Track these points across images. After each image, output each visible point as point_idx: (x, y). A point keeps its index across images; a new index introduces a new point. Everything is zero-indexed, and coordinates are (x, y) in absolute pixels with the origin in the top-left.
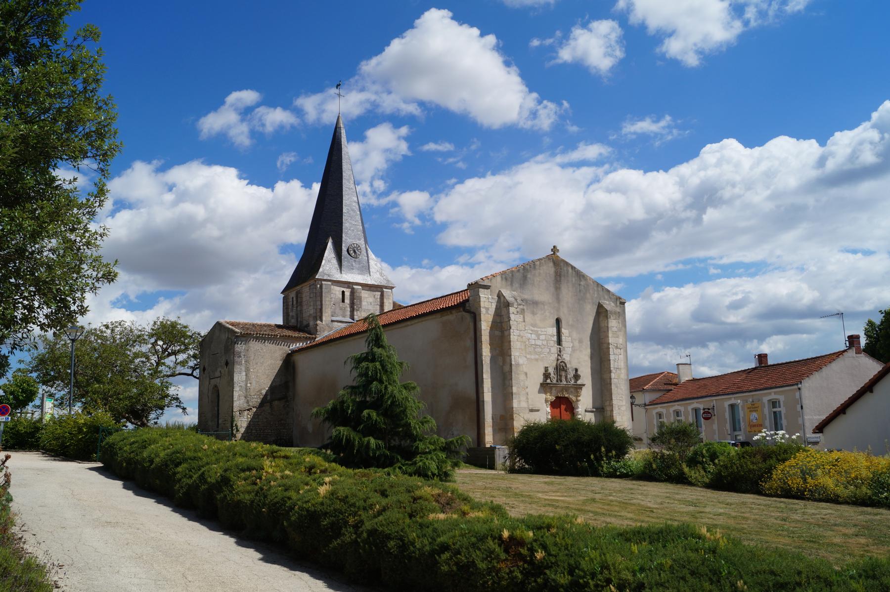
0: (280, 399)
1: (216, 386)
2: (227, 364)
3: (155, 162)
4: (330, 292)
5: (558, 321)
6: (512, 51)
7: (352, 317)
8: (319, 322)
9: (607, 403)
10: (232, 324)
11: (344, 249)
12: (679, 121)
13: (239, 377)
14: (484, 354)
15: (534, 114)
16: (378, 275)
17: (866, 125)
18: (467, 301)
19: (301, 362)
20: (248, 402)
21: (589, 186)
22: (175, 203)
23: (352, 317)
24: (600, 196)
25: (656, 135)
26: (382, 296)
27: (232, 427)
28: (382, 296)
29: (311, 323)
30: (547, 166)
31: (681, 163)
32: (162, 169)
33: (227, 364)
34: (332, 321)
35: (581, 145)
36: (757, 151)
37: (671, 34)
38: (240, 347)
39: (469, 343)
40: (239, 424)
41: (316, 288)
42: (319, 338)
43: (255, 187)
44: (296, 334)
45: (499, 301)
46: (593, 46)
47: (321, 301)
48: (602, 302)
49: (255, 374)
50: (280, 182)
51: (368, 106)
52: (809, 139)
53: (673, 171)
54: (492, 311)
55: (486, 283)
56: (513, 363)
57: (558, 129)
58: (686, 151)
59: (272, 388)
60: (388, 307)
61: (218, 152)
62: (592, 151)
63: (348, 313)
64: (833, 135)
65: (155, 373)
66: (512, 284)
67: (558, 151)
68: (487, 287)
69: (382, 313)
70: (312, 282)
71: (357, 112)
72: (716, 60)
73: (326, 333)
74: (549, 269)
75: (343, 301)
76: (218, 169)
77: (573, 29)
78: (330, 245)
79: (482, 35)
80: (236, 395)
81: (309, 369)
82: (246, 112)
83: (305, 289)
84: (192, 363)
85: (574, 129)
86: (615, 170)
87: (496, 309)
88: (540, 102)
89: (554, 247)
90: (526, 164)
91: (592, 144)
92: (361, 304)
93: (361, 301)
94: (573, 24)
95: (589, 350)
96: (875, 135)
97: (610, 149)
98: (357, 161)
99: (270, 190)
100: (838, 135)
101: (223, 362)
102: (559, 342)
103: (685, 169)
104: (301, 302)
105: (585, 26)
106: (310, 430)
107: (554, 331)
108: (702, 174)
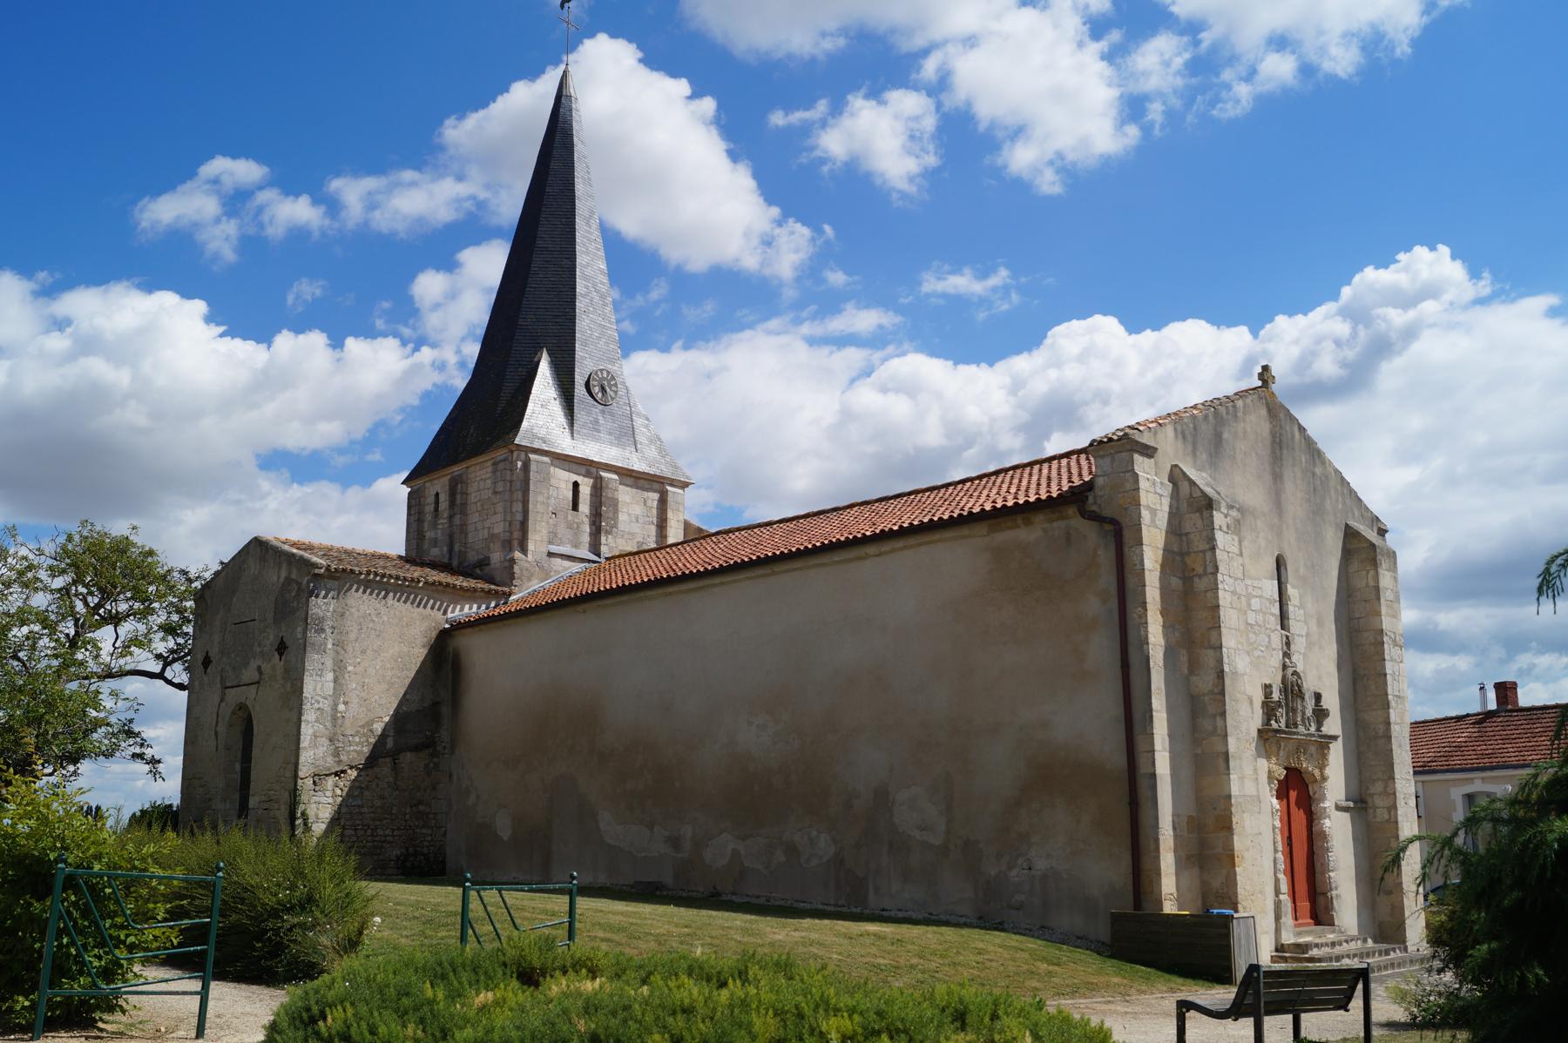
0: (416, 749)
1: (242, 707)
2: (282, 648)
3: (42, 275)
4: (546, 479)
5: (1280, 563)
6: (742, 133)
7: (595, 548)
8: (517, 554)
9: (1378, 787)
10: (294, 545)
11: (580, 381)
12: (1023, 280)
13: (317, 686)
14: (1151, 639)
15: (768, 242)
16: (652, 452)
17: (1329, 307)
18: (1088, 486)
19: (479, 652)
20: (336, 753)
21: (853, 381)
22: (71, 357)
23: (595, 548)
24: (866, 397)
25: (983, 302)
26: (663, 502)
27: (293, 818)
28: (663, 502)
29: (496, 557)
30: (784, 339)
31: (1018, 352)
32: (49, 292)
33: (282, 648)
34: (550, 554)
35: (850, 307)
36: (1148, 337)
37: (1018, 132)
38: (322, 606)
39: (1095, 605)
40: (311, 813)
41: (512, 469)
42: (520, 595)
43: (238, 342)
44: (459, 581)
45: (1175, 494)
46: (880, 136)
47: (525, 503)
48: (1351, 523)
49: (356, 678)
50: (285, 332)
51: (468, 205)
52: (1235, 325)
53: (1001, 366)
54: (1163, 519)
55: (1146, 439)
56: (1226, 668)
57: (811, 271)
58: (1022, 333)
59: (400, 719)
60: (675, 534)
61: (170, 265)
62: (866, 320)
63: (586, 538)
64: (1271, 320)
65: (68, 665)
66: (1194, 453)
67: (804, 314)
68: (1149, 451)
69: (662, 545)
70: (500, 454)
71: (445, 215)
72: (1090, 184)
73: (535, 585)
74: (1256, 423)
75: (575, 507)
76: (167, 299)
77: (850, 97)
78: (544, 370)
79: (695, 95)
80: (307, 731)
81: (501, 674)
82: (236, 200)
83: (480, 474)
84: (162, 645)
85: (837, 278)
86: (903, 354)
87: (1171, 515)
88: (780, 223)
89: (1265, 368)
90: (747, 334)
91: (867, 307)
92: (616, 518)
93: (616, 511)
94: (855, 88)
95: (1334, 647)
96: (1342, 328)
97: (898, 319)
98: (437, 306)
99: (263, 346)
100: (1281, 321)
101: (270, 639)
102: (1283, 617)
103: (1021, 363)
104: (464, 505)
105: (875, 94)
106: (505, 834)
107: (1271, 587)
108: (1053, 374)
